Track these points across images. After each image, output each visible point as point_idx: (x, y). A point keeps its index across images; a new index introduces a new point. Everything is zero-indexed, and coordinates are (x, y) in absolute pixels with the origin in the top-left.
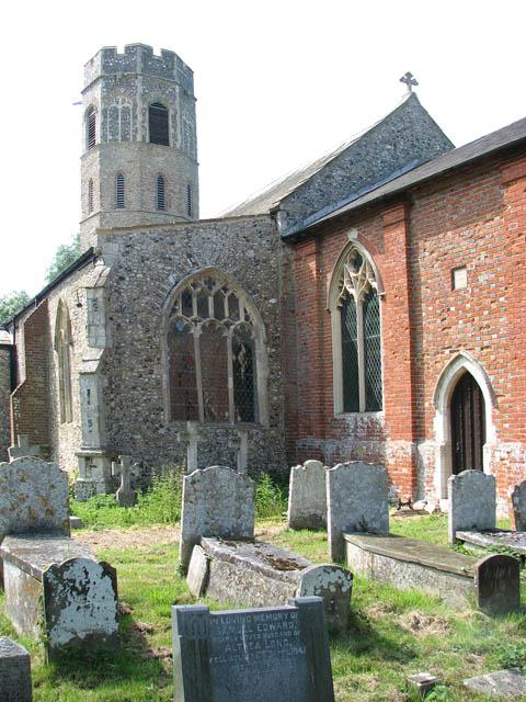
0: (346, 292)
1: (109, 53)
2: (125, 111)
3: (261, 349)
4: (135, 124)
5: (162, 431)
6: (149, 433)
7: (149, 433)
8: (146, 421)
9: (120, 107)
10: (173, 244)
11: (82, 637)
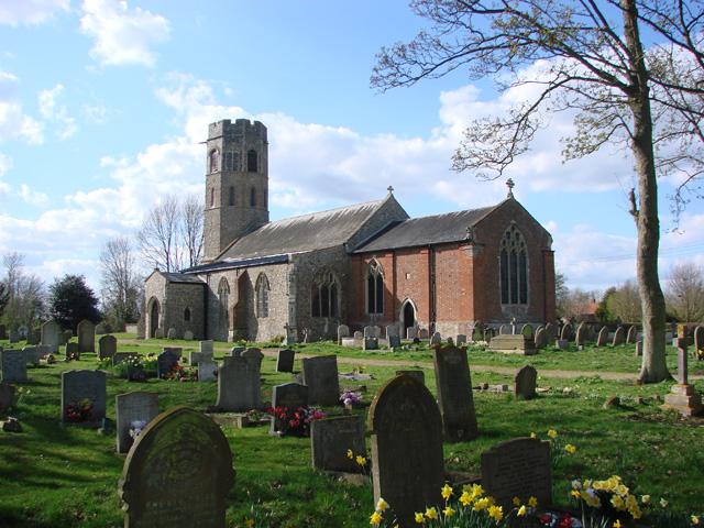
1: (227, 123)
3: (339, 291)
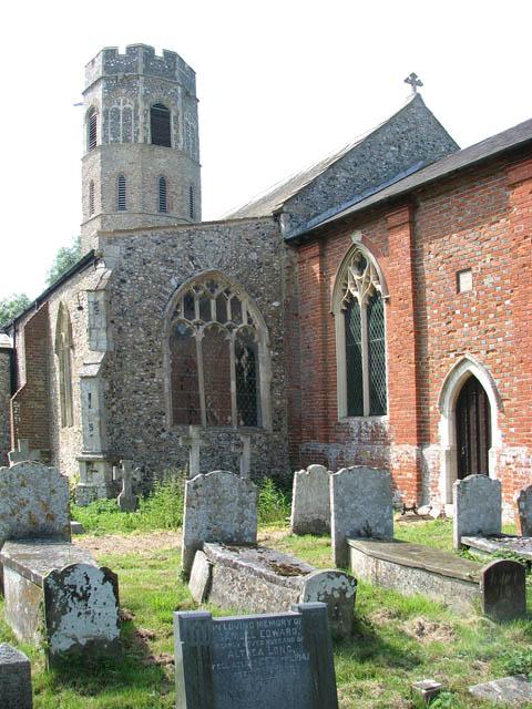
0: (350, 295)
1: (110, 54)
2: (127, 112)
3: (264, 353)
4: (136, 125)
5: (163, 435)
6: (151, 437)
7: (151, 437)
8: (147, 425)
9: (121, 108)
10: (175, 246)
11: (83, 644)
